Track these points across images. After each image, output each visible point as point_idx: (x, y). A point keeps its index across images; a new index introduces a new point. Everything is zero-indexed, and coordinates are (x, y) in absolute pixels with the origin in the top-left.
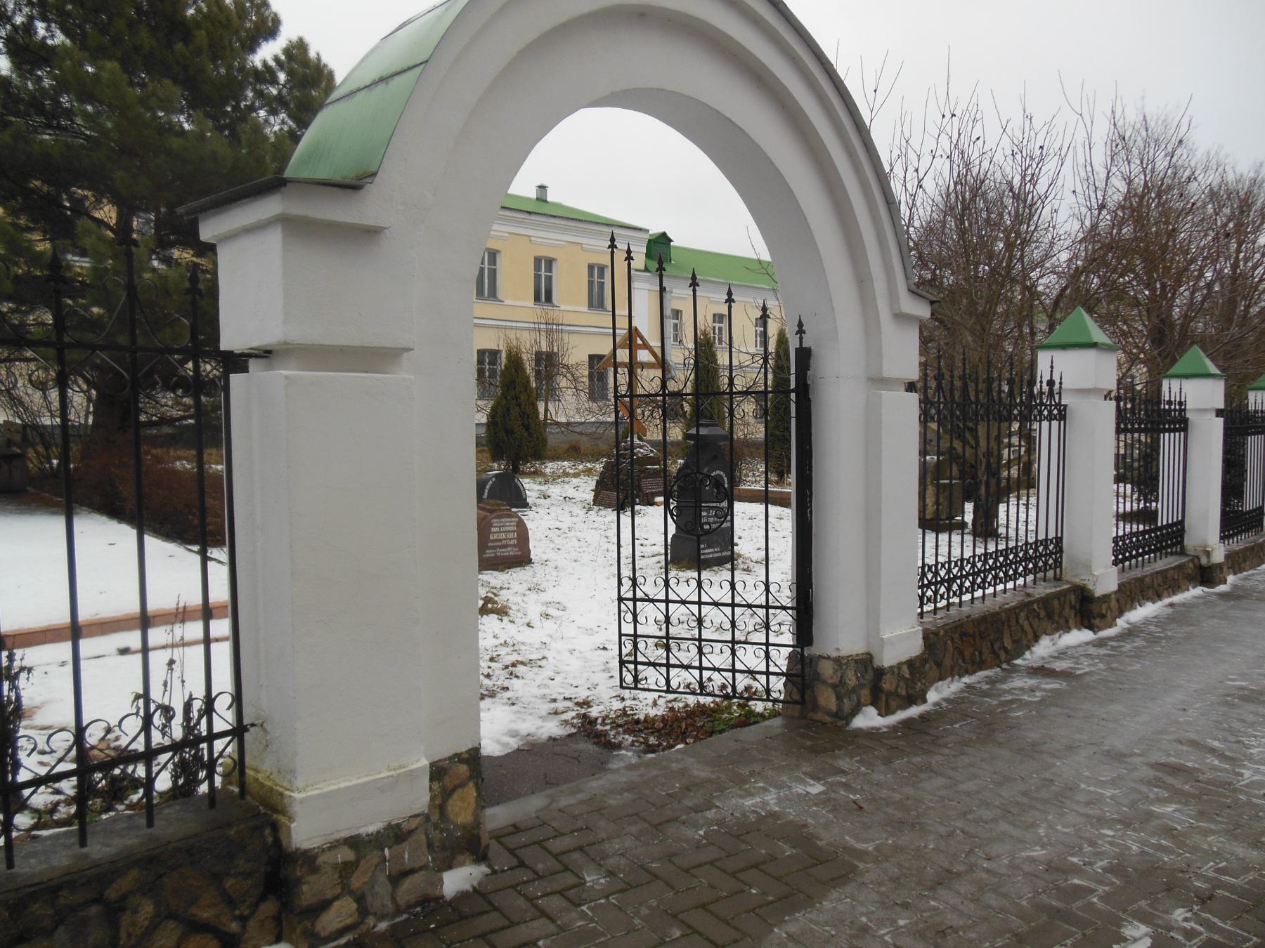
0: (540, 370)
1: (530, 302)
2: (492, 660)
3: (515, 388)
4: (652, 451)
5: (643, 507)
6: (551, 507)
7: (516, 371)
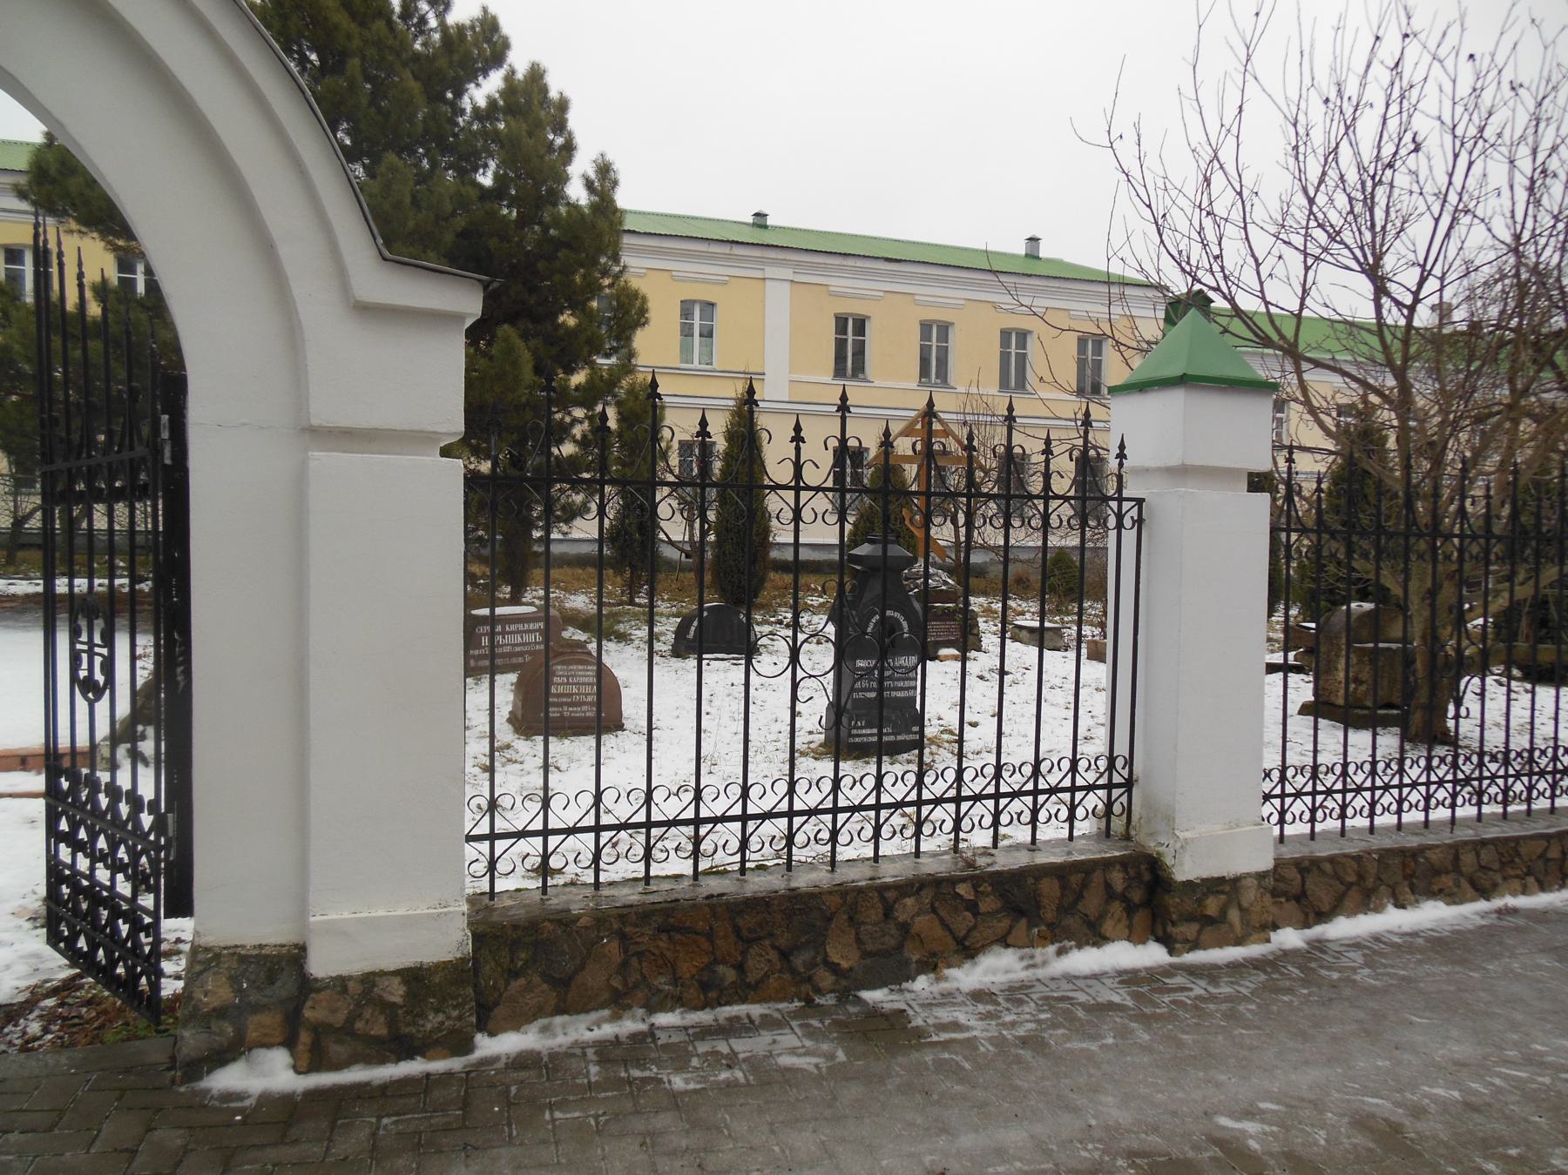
1: (828, 378)
4: (945, 583)
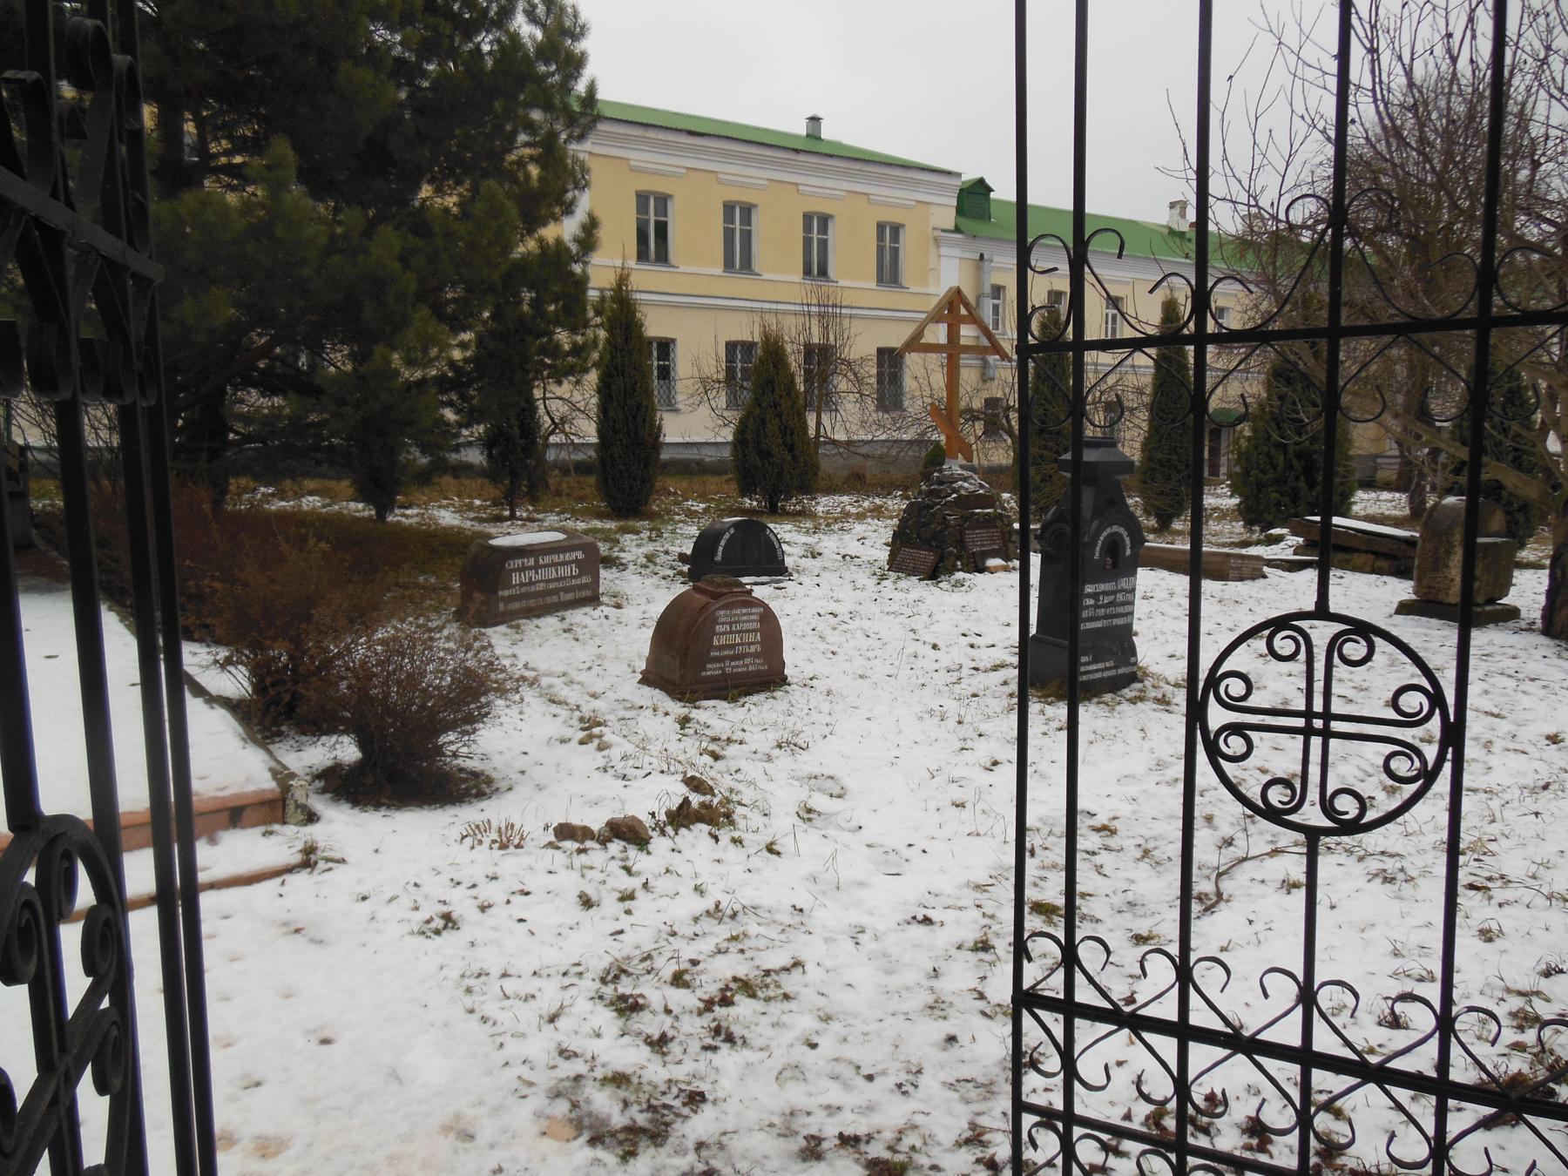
0: (811, 371)
1: (798, 277)
2: (678, 980)
3: (773, 392)
4: (982, 486)
5: (967, 576)
6: (822, 574)
7: (775, 366)
